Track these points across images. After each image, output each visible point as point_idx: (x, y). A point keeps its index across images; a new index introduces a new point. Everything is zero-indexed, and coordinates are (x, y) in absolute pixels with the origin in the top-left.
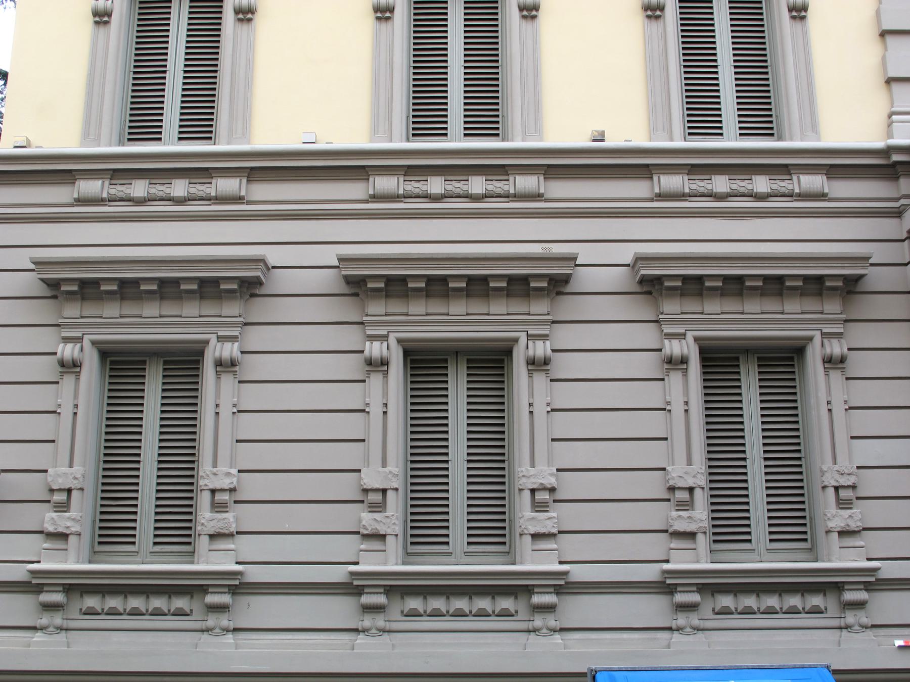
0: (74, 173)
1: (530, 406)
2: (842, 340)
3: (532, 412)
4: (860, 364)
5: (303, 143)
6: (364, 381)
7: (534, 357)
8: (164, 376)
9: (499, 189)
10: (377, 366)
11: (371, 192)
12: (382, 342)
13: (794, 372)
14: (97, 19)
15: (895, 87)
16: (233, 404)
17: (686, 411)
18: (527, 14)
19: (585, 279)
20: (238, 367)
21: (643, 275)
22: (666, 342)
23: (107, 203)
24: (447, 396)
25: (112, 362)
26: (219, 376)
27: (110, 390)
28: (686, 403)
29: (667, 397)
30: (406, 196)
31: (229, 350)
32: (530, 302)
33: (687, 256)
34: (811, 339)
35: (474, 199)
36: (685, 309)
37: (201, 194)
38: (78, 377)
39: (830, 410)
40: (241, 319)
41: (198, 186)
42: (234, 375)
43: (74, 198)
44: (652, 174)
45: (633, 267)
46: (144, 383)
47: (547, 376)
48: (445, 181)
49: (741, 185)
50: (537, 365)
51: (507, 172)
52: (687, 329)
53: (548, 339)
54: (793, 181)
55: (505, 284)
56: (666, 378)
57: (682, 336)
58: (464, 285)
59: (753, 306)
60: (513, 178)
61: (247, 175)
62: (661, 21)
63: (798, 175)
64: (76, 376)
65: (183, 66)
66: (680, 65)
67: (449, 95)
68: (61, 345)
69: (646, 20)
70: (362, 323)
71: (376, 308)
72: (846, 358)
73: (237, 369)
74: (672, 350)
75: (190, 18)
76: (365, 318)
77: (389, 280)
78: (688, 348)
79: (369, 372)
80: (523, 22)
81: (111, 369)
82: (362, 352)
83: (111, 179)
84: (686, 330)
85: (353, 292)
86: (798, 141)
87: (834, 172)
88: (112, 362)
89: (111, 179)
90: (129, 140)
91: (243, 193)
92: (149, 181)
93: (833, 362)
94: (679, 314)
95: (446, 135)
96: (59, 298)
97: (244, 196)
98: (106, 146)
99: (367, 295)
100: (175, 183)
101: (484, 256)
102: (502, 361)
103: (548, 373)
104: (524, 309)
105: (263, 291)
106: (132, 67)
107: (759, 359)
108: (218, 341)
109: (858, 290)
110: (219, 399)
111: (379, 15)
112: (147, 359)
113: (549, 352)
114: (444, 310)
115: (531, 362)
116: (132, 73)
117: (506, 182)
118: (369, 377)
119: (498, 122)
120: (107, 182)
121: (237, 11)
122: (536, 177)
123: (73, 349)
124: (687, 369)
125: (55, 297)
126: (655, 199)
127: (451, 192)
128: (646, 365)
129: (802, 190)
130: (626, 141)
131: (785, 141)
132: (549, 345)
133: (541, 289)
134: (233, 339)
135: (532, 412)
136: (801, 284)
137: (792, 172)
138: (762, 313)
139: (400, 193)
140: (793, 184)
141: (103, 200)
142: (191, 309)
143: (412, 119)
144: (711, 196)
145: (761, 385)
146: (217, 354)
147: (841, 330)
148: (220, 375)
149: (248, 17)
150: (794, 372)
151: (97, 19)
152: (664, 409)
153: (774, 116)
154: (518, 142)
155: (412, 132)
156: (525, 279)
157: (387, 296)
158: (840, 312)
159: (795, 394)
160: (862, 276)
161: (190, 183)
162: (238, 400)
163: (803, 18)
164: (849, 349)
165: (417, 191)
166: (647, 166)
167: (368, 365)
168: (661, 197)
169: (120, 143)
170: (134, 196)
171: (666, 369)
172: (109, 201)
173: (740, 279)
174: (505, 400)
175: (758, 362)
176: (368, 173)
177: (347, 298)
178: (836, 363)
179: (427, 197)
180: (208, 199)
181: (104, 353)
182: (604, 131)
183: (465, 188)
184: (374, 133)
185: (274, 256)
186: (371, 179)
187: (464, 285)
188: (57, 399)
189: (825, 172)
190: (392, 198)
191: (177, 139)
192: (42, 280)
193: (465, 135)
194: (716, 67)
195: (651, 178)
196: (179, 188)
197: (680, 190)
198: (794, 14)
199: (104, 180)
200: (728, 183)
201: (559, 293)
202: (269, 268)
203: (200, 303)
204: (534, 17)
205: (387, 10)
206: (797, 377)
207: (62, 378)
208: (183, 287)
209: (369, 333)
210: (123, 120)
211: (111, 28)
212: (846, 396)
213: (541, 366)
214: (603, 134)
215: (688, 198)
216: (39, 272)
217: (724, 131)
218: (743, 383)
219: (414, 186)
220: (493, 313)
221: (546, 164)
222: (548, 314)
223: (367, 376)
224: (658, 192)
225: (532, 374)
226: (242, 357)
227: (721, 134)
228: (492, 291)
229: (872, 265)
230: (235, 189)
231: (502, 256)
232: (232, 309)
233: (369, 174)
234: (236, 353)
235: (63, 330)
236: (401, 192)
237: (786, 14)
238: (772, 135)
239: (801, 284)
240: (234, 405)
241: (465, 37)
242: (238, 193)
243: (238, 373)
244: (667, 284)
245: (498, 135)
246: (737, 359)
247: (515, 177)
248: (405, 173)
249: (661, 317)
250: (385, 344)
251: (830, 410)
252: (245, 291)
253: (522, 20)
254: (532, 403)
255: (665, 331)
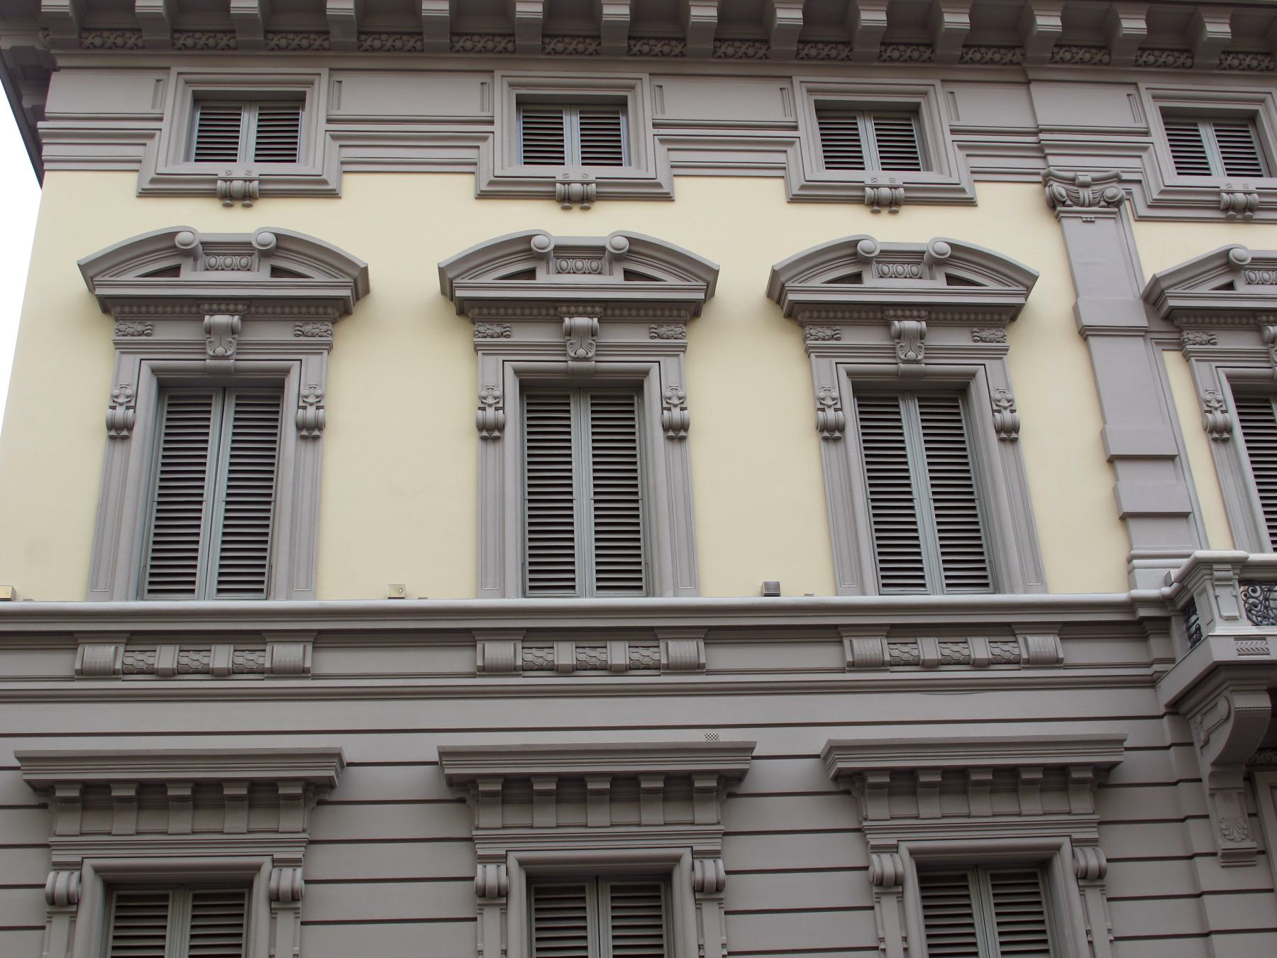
0: (76, 635)
1: (700, 949)
2: (1097, 848)
3: (1091, 942)
4: (1125, 879)
5: (389, 598)
6: (475, 919)
7: (53, 894)
8: (194, 917)
9: (957, 653)
10: (492, 898)
11: (480, 663)
12: (295, 868)
13: (1038, 893)
14: (113, 433)
15: (1133, 524)
16: (722, 945)
17: (906, 950)
18: (487, 435)
19: (765, 775)
20: (301, 902)
21: (840, 770)
22: (874, 857)
23: (120, 676)
24: (585, 938)
25: (120, 898)
26: (274, 916)
27: (115, 938)
28: (905, 939)
29: (879, 932)
30: (893, 663)
31: (289, 879)
32: (693, 807)
33: (638, 748)
34: (1058, 848)
35: (561, 672)
36: (617, 820)
37: (140, 665)
38: (73, 919)
39: (1090, 943)
40: (305, 835)
41: (192, 655)
42: (719, 904)
43: (479, 666)
44: (842, 637)
45: (825, 759)
46: (165, 927)
47: (1102, 894)
48: (576, 648)
49: (954, 650)
50: (707, 892)
51: (840, 634)
52: (509, 849)
53: (719, 858)
54: (1019, 644)
55: (553, 787)
56: (877, 906)
57: (893, 849)
58: (500, 788)
59: (982, 807)
60: (482, 645)
61: (312, 640)
62: (841, 445)
63: (1024, 636)
64: (501, 909)
65: (225, 495)
66: (867, 498)
67: (575, 536)
68: (52, 874)
69: (823, 444)
70: (470, 839)
71: (490, 819)
72: (724, 885)
73: (299, 905)
74: (882, 867)
75: (234, 434)
76: (475, 833)
77: (508, 780)
78: (900, 864)
79: (51, 915)
80: (670, 444)
81: (118, 907)
82: (472, 879)
83: (126, 644)
84: (898, 841)
85: (458, 797)
86: (1021, 593)
87: (1068, 631)
88: (120, 898)
89: (126, 644)
90: (150, 591)
91: (308, 664)
92: (234, 647)
93: (1090, 879)
94: (888, 820)
95: (573, 587)
96: (49, 807)
97: (1062, 659)
98: (121, 600)
99: (478, 801)
100: (215, 649)
101: (633, 748)
102: (657, 888)
103: (1103, 890)
104: (160, 826)
105: (335, 796)
106: (156, 495)
107: (993, 877)
108: (274, 867)
109: (1111, 782)
110: (275, 947)
111: (485, 434)
112: (170, 892)
113: (722, 874)
114: (581, 820)
115: (700, 889)
116: (156, 503)
117: (656, 650)
118: (482, 914)
119: (640, 571)
120: (121, 649)
121: (300, 426)
122: (695, 642)
123: (69, 879)
124: (902, 893)
125: (43, 806)
126: (847, 669)
127: (897, 659)
128: (454, 899)
129: (1031, 655)
130: (806, 595)
131: (1004, 593)
132: (722, 864)
133: (122, 800)
134: (294, 863)
135: (1091, 942)
136: (939, 779)
137: (1016, 632)
138: (994, 816)
139: (886, 659)
140: (1019, 647)
141: (115, 672)
142: (236, 823)
143: (528, 568)
144: (917, 664)
145: (997, 911)
146: (273, 884)
147: (1096, 836)
148: (276, 913)
149: (122, 434)
150: (1038, 893)
151: (113, 433)
152: (876, 948)
153: (987, 561)
154: (669, 597)
155: (528, 584)
156: (687, 778)
157: (251, 806)
158: (1091, 812)
159: (1042, 922)
160: (1115, 764)
161: (126, 651)
162: (300, 950)
163: (1014, 441)
164: (1109, 860)
165: (195, 665)
166: (835, 627)
167: (480, 896)
168: (486, 670)
169: (137, 595)
170: (160, 667)
171: (876, 893)
172: (124, 674)
173: (912, 773)
174: (664, 941)
175: (992, 880)
176: (474, 638)
177: (36, 811)
178: (1092, 880)
179: (969, 664)
180: (261, 672)
181: (109, 884)
182: (779, 583)
183: (603, 657)
184: (481, 586)
185: (352, 748)
186: (479, 646)
187: (500, 788)
188: (42, 951)
189: (703, 636)
190: (690, 668)
191: (215, 590)
192: (29, 782)
193: (599, 588)
194: (571, 501)
195: (841, 642)
196: (221, 657)
197: (879, 657)
198: (1003, 435)
199: (305, 644)
200: (988, 646)
201: (732, 795)
202: (344, 765)
203: (193, 816)
204: (316, 438)
205: (495, 428)
206: (1043, 899)
207: (482, 914)
208: (170, 793)
209: (480, 852)
210: (142, 565)
211: (132, 447)
212: (1109, 923)
213: (711, 893)
214: (777, 586)
215: (889, 668)
216: (27, 772)
217: (927, 581)
218: (975, 910)
219: (138, 659)
220: (976, 815)
221: (129, 631)
222: (718, 823)
223: (478, 911)
224: (481, 664)
225: (701, 904)
226: (306, 888)
227: (923, 585)
228: (172, 801)
229: (1127, 749)
230: (108, 660)
231: (657, 747)
232: (292, 822)
233: (476, 638)
234: (299, 883)
235: (54, 852)
236: (519, 662)
237: (659, 434)
238: (986, 585)
239: (939, 779)
240: (724, 946)
241: (594, 463)
242: (301, 663)
243: (300, 911)
244: (871, 780)
245: (640, 588)
246: (964, 878)
247: (484, 645)
248: (524, 637)
249: (865, 823)
250: (503, 867)
251: (1090, 943)
252: (311, 796)
253: (667, 441)
254: (703, 945)
255: (872, 842)
